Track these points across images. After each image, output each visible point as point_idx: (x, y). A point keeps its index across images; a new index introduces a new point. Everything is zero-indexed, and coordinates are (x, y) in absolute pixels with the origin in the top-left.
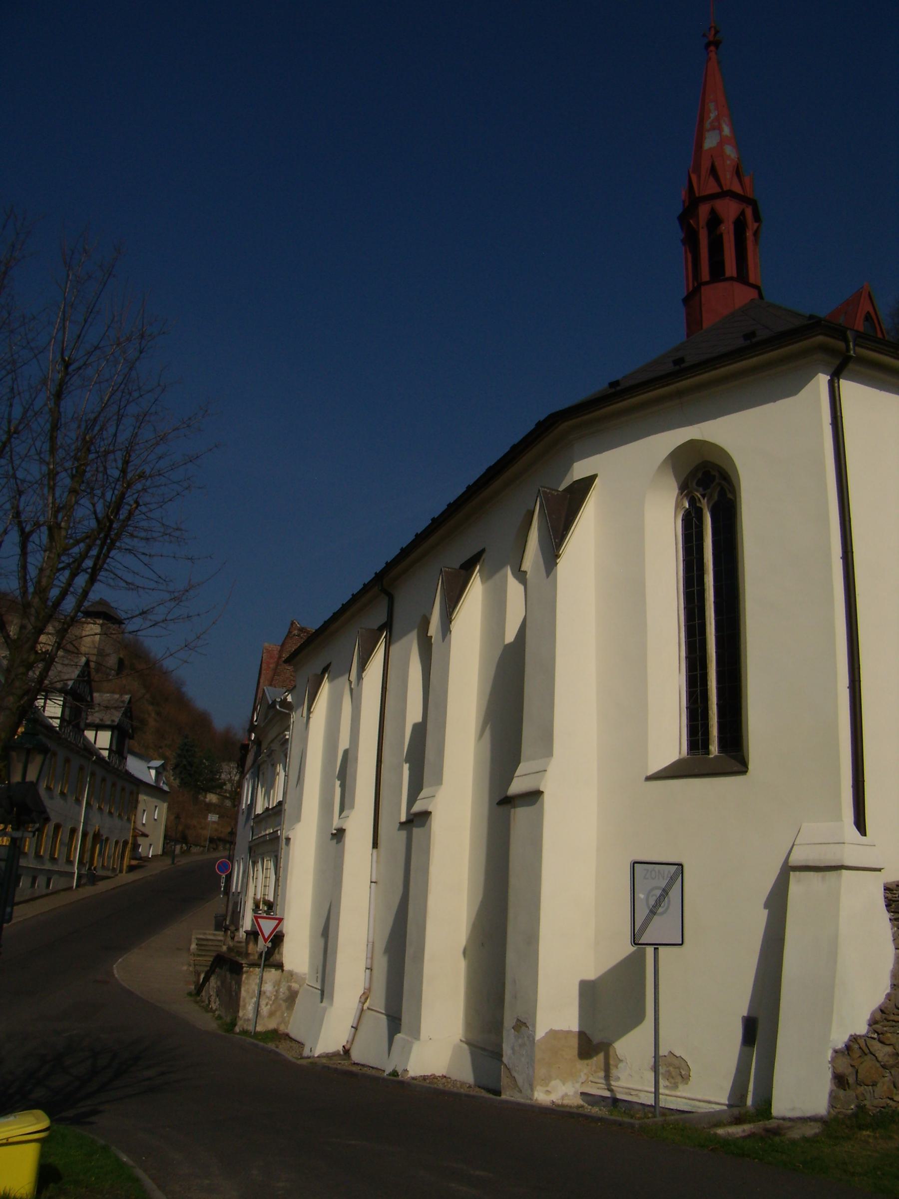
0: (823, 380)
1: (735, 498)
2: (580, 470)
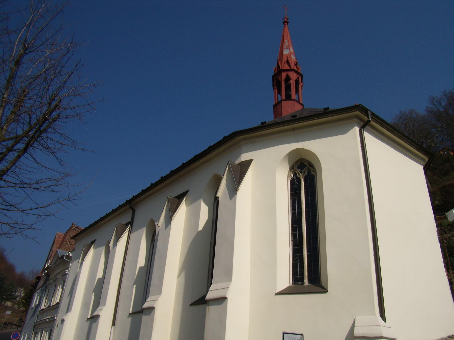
0: (357, 129)
1: (316, 174)
2: (244, 157)
